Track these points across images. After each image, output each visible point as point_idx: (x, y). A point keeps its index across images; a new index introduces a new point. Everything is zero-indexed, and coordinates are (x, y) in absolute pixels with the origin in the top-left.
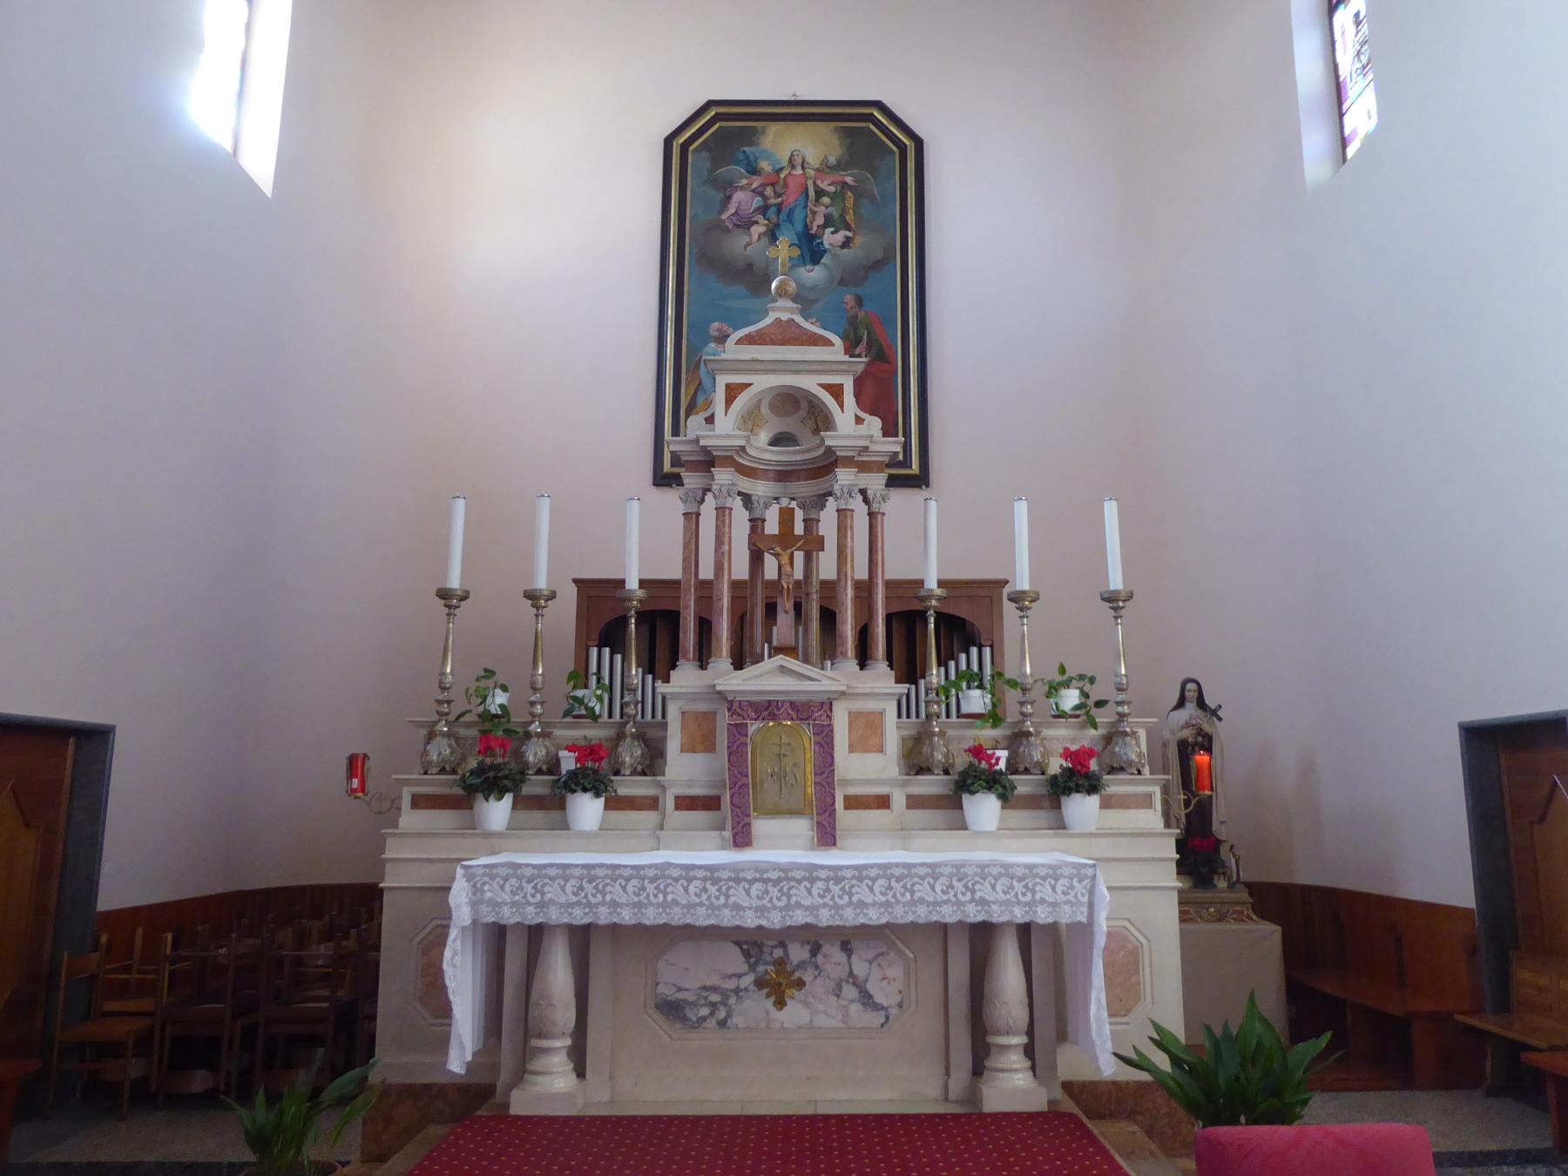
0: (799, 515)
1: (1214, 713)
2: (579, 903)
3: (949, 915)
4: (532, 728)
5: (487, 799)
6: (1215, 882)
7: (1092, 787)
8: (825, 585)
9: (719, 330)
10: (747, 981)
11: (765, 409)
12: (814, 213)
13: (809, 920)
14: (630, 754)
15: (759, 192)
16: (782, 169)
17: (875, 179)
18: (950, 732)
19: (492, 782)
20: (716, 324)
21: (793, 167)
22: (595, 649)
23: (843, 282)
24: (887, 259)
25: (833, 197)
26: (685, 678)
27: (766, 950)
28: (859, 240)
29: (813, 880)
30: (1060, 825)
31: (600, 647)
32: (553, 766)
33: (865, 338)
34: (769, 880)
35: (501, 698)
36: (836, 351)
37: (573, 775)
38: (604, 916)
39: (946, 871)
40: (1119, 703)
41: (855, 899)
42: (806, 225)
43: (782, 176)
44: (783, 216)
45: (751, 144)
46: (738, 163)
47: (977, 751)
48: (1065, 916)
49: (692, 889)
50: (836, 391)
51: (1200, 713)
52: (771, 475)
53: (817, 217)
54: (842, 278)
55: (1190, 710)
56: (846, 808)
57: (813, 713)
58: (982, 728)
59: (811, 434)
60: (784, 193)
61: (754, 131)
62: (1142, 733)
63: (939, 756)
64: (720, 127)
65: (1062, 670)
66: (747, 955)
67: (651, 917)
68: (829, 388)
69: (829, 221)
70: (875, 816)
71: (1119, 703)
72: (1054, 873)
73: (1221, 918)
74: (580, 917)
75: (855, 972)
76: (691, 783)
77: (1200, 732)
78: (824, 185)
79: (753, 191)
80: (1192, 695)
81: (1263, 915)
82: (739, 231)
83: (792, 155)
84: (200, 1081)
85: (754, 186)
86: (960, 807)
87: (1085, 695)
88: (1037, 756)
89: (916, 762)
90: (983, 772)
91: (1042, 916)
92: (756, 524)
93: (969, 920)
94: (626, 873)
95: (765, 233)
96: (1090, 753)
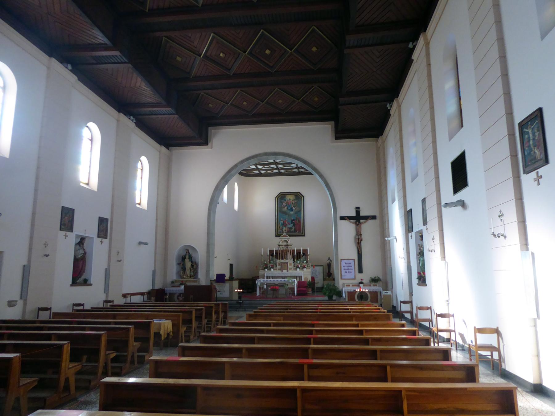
1: (331, 261)
3: (294, 275)
7: (305, 268)
14: (275, 266)
15: (286, 203)
23: (295, 213)
24: (300, 211)
28: (297, 209)
30: (303, 270)
32: (270, 267)
35: (266, 262)
38: (274, 276)
48: (301, 275)
55: (329, 260)
57: (287, 263)
61: (286, 196)
69: (294, 206)
70: (291, 270)
72: (300, 273)
74: (272, 276)
77: (330, 263)
80: (329, 259)
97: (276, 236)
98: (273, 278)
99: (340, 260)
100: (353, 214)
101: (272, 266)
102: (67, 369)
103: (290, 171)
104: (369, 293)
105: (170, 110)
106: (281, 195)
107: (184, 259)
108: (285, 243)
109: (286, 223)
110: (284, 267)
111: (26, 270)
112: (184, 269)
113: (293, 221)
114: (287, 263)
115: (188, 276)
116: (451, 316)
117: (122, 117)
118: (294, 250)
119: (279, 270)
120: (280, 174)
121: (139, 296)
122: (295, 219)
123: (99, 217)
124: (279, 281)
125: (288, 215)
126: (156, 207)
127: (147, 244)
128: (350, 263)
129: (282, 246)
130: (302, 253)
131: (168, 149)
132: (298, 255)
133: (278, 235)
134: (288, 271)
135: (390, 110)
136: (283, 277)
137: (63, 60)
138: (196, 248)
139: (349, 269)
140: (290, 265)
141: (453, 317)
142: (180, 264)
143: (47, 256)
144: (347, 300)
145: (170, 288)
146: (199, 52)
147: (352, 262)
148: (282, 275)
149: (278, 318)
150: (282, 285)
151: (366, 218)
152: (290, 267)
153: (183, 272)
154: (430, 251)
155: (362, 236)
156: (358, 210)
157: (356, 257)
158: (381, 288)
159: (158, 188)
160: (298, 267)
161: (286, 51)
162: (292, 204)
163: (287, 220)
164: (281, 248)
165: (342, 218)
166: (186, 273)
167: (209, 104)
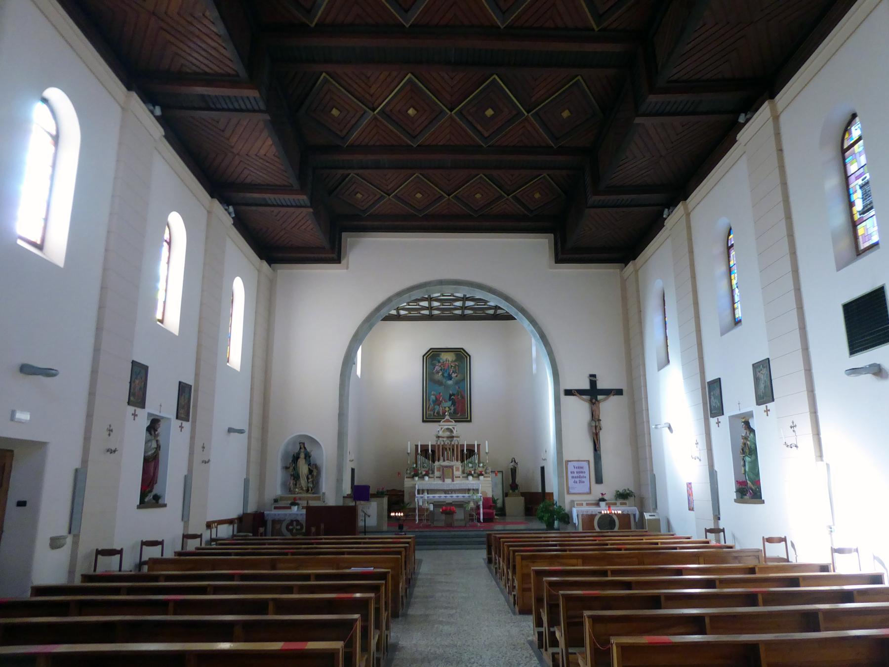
1: (517, 464)
3: (465, 488)
7: (482, 475)
14: (430, 472)
15: (440, 366)
19: (416, 475)
26: (437, 463)
28: (459, 376)
30: (479, 479)
32: (421, 473)
48: (477, 488)
55: (513, 463)
57: (451, 467)
70: (459, 479)
72: (475, 484)
74: (428, 488)
77: (514, 466)
80: (514, 461)
81: (522, 496)
89: (463, 472)
98: (429, 492)
99: (566, 461)
100: (586, 386)
101: (426, 472)
103: (448, 313)
104: (617, 516)
105: (304, 198)
106: (433, 351)
107: (296, 458)
108: (448, 434)
109: (441, 399)
110: (446, 473)
111: (79, 477)
112: (296, 477)
113: (453, 397)
114: (451, 467)
115: (304, 489)
116: (854, 552)
117: (217, 206)
118: (464, 445)
119: (437, 479)
120: (431, 318)
121: (225, 526)
122: (455, 393)
123: (180, 383)
124: (459, 497)
126: (250, 365)
127: (242, 433)
128: (582, 468)
129: (443, 437)
130: (430, 451)
131: (270, 266)
132: (468, 453)
133: (427, 419)
134: (453, 481)
135: (666, 219)
136: (446, 492)
137: (149, 98)
138: (318, 440)
139: (580, 477)
140: (456, 471)
141: (856, 553)
142: (289, 468)
143: (113, 451)
144: (580, 530)
145: (271, 511)
146: (373, 104)
147: (585, 464)
148: (445, 488)
149: (574, 561)
150: (461, 505)
151: (608, 392)
152: (456, 473)
153: (295, 482)
154: (788, 446)
155: (601, 422)
156: (593, 379)
157: (590, 457)
158: (636, 508)
159: (255, 334)
160: (470, 474)
161: (442, 111)
162: (451, 368)
163: (441, 394)
164: (441, 442)
165: (568, 393)
166: (300, 484)
167: (357, 193)
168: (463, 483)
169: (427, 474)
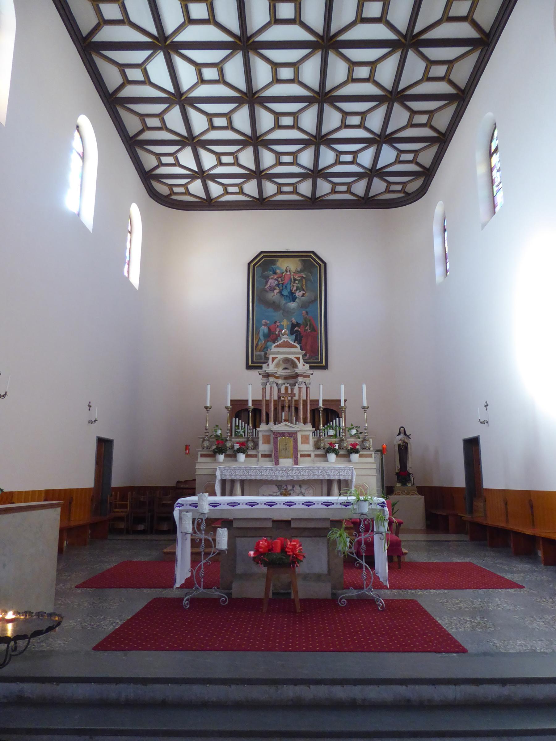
0: (289, 388)
1: (408, 437)
2: (243, 475)
3: (321, 477)
4: (227, 439)
5: (219, 454)
6: (407, 484)
7: (357, 452)
8: (296, 401)
9: (265, 322)
10: (279, 493)
11: (281, 362)
12: (293, 286)
13: (292, 478)
14: (250, 445)
15: (276, 280)
16: (283, 272)
17: (311, 274)
18: (325, 440)
19: (220, 450)
20: (264, 320)
21: (287, 272)
22: (234, 419)
23: (302, 307)
24: (316, 300)
25: (299, 281)
26: (263, 427)
27: (283, 487)
28: (307, 294)
29: (293, 470)
30: (350, 461)
31: (235, 418)
32: (232, 447)
33: (309, 324)
34: (283, 470)
35: (219, 432)
36: (298, 349)
37: (238, 449)
38: (249, 478)
39: (321, 468)
40: (365, 433)
41: (302, 474)
42: (291, 290)
43: (284, 274)
44: (284, 287)
45: (274, 264)
46: (270, 271)
47: (331, 444)
49: (267, 472)
50: (298, 359)
51: (405, 436)
52: (283, 378)
53: (294, 287)
54: (302, 306)
55: (402, 436)
56: (301, 457)
57: (293, 435)
58: (332, 439)
59: (292, 368)
60: (284, 280)
62: (371, 440)
63: (322, 445)
64: (265, 260)
65: (352, 425)
66: (278, 488)
67: (259, 478)
68: (296, 358)
71: (365, 433)
73: (408, 494)
74: (243, 478)
75: (302, 492)
76: (265, 451)
77: (404, 442)
78: (296, 277)
79: (275, 279)
80: (403, 431)
82: (271, 292)
83: (286, 268)
84: (141, 527)
85: (275, 278)
86: (327, 457)
87: (357, 431)
88: (345, 445)
90: (332, 448)
91: (342, 478)
92: (279, 390)
93: (326, 479)
94: (253, 468)
95: (278, 292)
96: (357, 444)
97: (248, 367)
98: (246, 488)
102: (273, 455)
109: (277, 333)
113: (296, 328)
114: (293, 435)
122: (300, 322)
125: (282, 311)
134: (296, 462)
148: (279, 476)
152: (304, 448)
160: (331, 449)
168: (318, 468)
169: (243, 449)
